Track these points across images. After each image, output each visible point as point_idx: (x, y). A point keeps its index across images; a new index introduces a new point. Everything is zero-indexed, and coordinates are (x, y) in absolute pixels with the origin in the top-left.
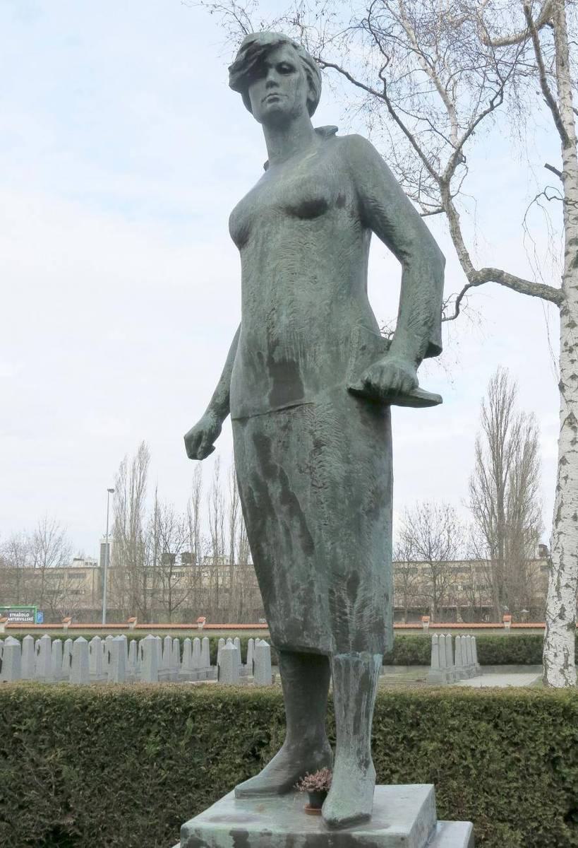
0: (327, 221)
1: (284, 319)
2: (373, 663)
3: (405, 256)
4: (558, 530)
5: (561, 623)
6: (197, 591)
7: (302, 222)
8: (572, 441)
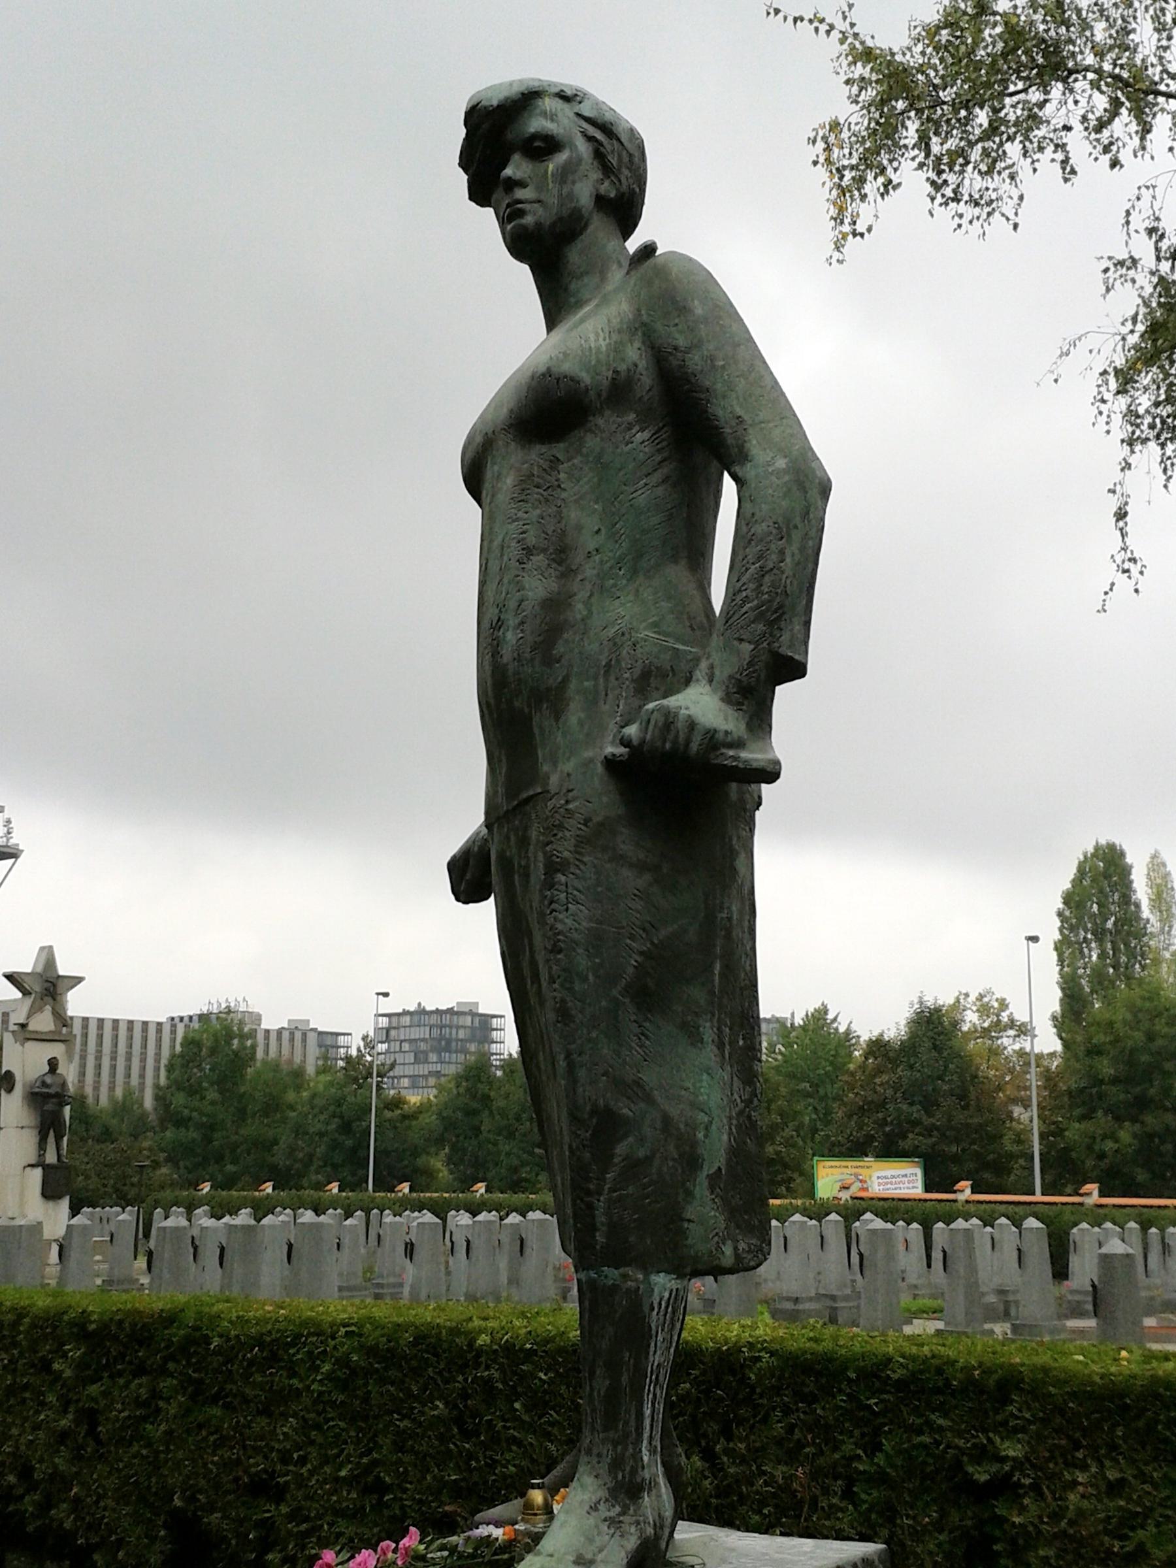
0: (589, 436)
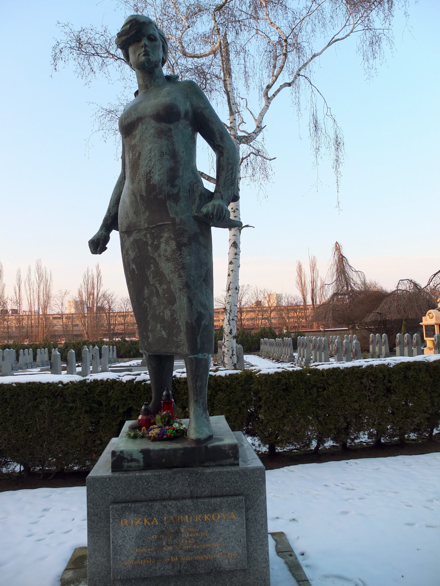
6: (20, 328)
8: (235, 254)
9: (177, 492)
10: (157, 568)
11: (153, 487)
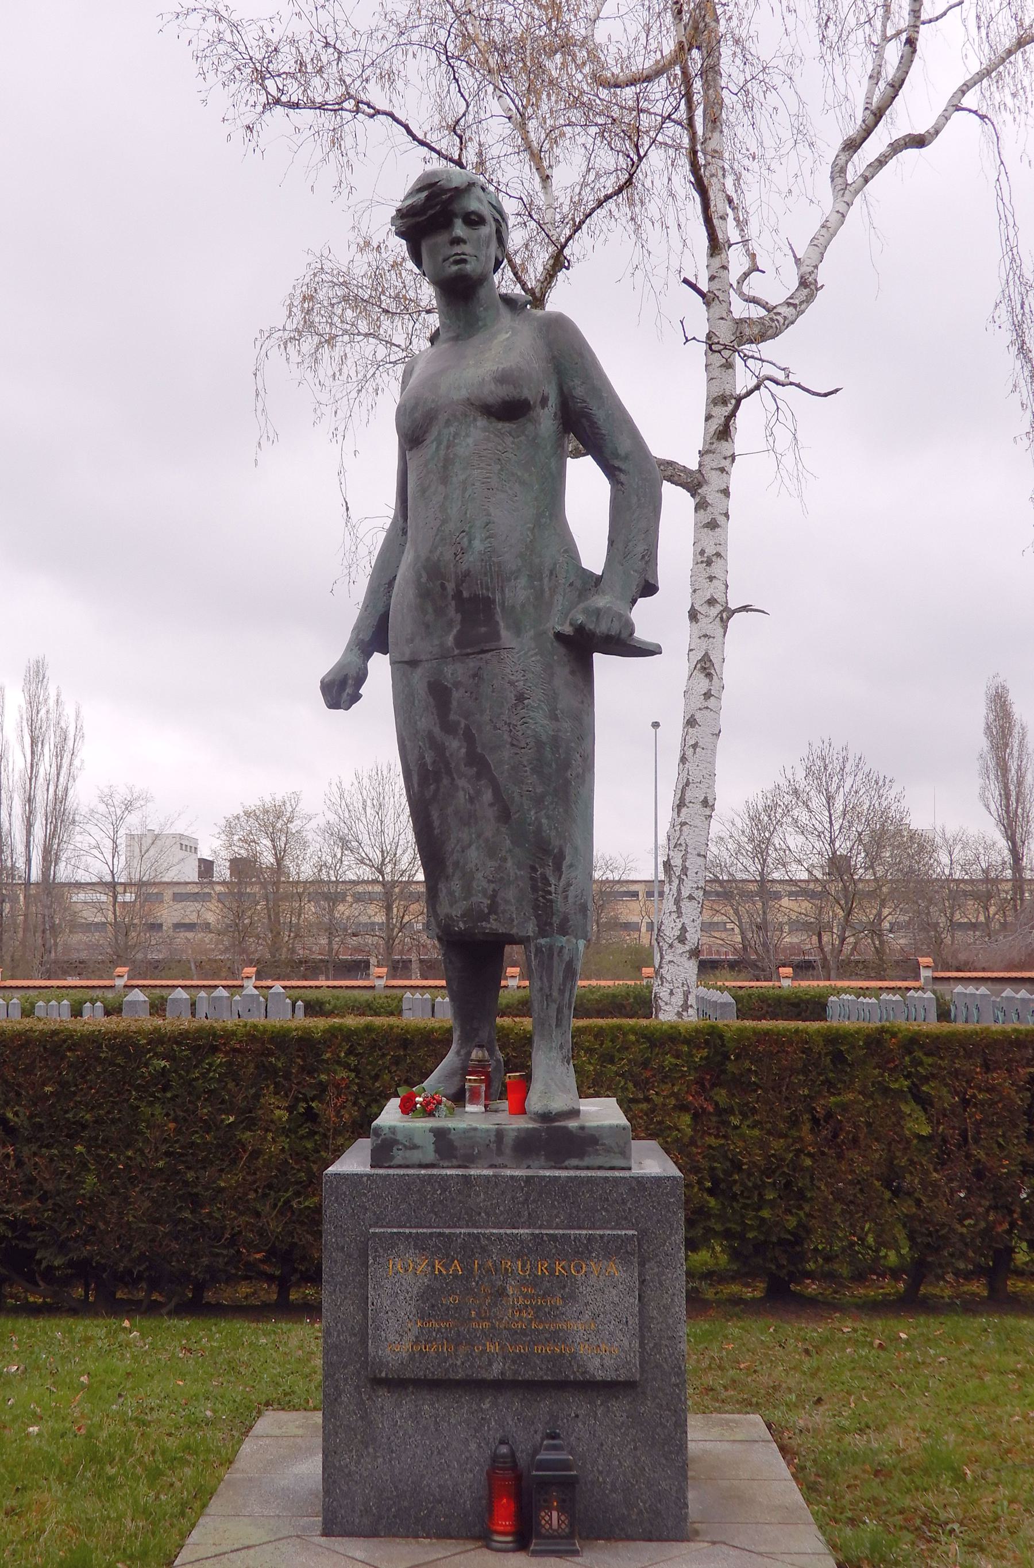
1: (477, 544)
2: (577, 948)
3: (617, 473)
4: (682, 819)
5: (680, 948)
7: (500, 425)
9: (502, 1213)
10: (459, 1363)
11: (453, 1199)
